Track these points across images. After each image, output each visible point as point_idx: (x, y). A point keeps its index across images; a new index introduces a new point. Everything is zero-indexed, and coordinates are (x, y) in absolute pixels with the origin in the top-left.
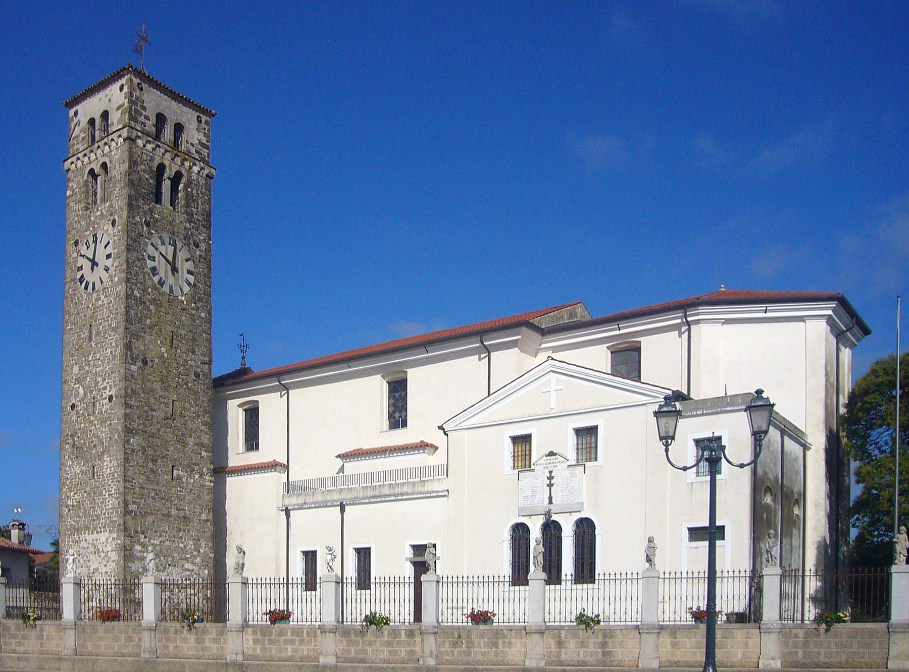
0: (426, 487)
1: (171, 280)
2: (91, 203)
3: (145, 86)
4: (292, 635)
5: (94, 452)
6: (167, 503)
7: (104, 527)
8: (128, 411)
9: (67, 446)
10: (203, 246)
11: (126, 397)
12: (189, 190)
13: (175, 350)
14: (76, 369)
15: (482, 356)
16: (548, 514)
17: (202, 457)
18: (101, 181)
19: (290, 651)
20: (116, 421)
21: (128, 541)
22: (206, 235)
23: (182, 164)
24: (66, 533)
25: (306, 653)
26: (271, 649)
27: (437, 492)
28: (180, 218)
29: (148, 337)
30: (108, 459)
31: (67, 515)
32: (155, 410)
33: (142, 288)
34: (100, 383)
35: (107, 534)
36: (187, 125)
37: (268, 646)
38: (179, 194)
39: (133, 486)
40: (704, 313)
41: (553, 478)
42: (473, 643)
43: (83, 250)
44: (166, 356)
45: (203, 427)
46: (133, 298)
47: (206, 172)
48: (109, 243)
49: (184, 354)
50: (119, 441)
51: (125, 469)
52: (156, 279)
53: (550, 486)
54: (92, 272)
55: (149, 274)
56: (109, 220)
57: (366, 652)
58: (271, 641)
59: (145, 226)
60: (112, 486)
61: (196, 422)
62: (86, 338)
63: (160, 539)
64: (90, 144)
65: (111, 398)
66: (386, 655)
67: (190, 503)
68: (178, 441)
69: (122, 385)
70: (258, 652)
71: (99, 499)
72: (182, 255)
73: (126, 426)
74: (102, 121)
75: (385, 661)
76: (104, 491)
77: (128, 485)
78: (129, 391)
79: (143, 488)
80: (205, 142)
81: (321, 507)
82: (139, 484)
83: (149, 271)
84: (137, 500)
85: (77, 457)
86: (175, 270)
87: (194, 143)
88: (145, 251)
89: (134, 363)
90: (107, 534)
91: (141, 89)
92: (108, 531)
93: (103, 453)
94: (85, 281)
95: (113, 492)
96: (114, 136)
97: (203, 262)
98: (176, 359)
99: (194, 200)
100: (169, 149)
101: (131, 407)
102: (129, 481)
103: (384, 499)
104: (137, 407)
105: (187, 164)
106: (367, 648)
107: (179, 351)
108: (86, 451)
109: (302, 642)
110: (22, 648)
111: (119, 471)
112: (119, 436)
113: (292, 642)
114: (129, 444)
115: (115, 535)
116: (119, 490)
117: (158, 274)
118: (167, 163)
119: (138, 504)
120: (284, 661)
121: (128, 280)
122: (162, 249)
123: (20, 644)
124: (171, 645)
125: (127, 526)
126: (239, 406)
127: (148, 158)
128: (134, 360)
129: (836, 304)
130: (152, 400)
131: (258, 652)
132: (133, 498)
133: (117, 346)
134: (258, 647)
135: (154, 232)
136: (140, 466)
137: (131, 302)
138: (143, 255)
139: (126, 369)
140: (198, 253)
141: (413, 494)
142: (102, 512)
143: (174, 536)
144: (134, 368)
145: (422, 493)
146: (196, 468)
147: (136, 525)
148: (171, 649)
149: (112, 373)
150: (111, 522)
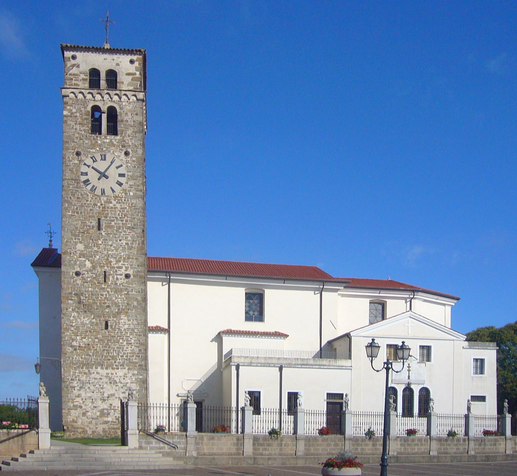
4: (418, 441)
16: (409, 384)
19: (416, 449)
25: (423, 450)
26: (408, 448)
27: (346, 367)
35: (126, 371)
37: (407, 447)
40: (420, 295)
41: (410, 367)
42: (486, 444)
53: (409, 371)
57: (447, 449)
58: (408, 445)
66: (454, 450)
70: (402, 450)
75: (455, 453)
81: (265, 366)
90: (126, 371)
106: (448, 447)
109: (422, 445)
110: (267, 452)
113: (418, 445)
115: (136, 372)
120: (414, 454)
123: (266, 450)
124: (359, 448)
129: (455, 303)
131: (402, 450)
134: (403, 448)
141: (329, 366)
148: (359, 451)
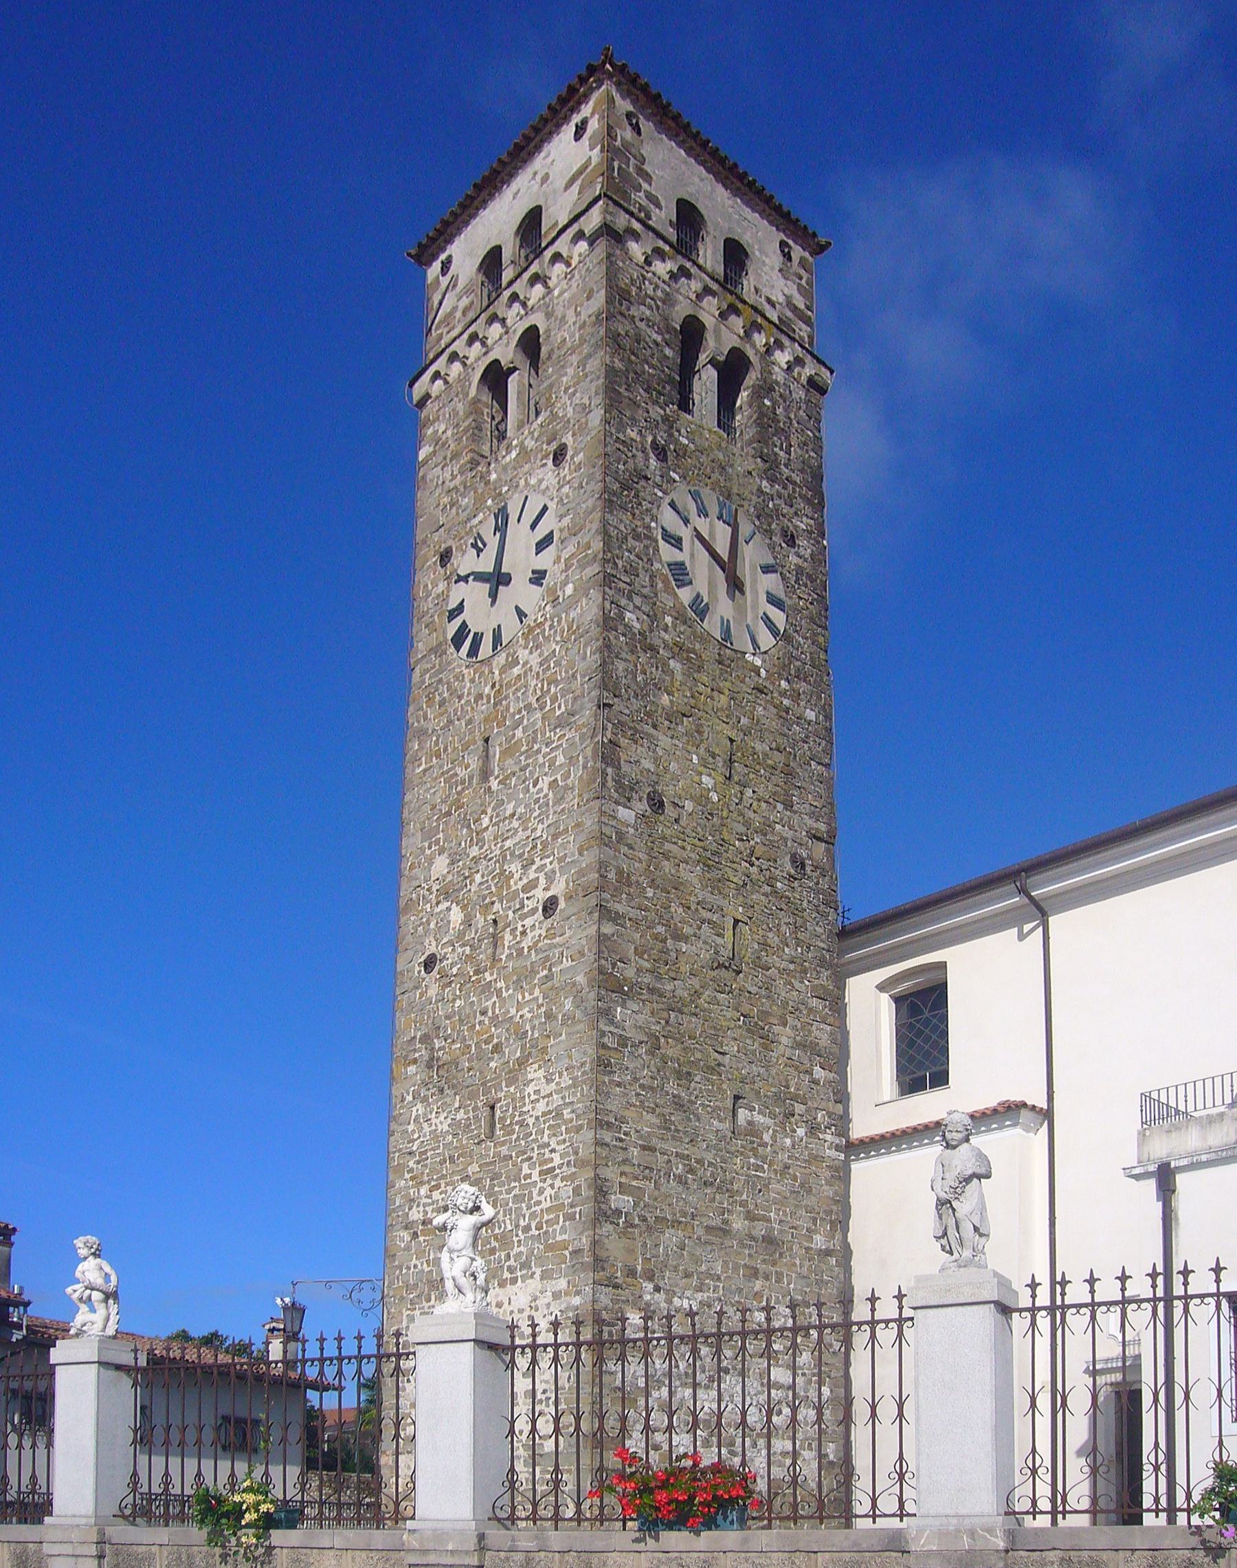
1: (724, 607)
2: (487, 454)
3: (647, 126)
5: (493, 1064)
6: (717, 1196)
7: (525, 1265)
8: (608, 929)
9: (412, 1069)
10: (805, 546)
11: (600, 889)
12: (767, 402)
13: (738, 788)
14: (441, 865)
17: (815, 1082)
18: (520, 382)
20: (566, 963)
21: (605, 1297)
22: (812, 522)
23: (748, 335)
24: (402, 1298)
28: (744, 462)
29: (664, 741)
30: (541, 1073)
31: (408, 1248)
32: (686, 939)
33: (646, 608)
34: (517, 876)
35: (534, 1284)
36: (757, 253)
38: (738, 418)
39: (621, 1140)
43: (466, 562)
44: (715, 798)
45: (814, 1002)
46: (621, 629)
47: (809, 370)
48: (545, 508)
49: (763, 805)
50: (578, 1014)
51: (600, 1091)
52: (685, 595)
54: (493, 603)
55: (666, 581)
56: (546, 456)
59: (652, 455)
60: (553, 1145)
61: (797, 985)
62: (471, 778)
63: (699, 1296)
64: (485, 303)
65: (550, 907)
67: (782, 1202)
68: (749, 1031)
69: (589, 858)
71: (509, 1192)
72: (752, 555)
73: (601, 971)
74: (521, 246)
76: (525, 1165)
77: (607, 1136)
78: (612, 875)
79: (652, 1149)
80: (802, 307)
82: (641, 1137)
83: (666, 571)
84: (634, 1183)
85: (442, 1091)
86: (735, 585)
87: (774, 298)
88: (654, 518)
89: (622, 800)
91: (637, 129)
92: (537, 1276)
93: (522, 1063)
94: (471, 635)
95: (557, 1160)
96: (562, 246)
97: (806, 586)
98: (741, 814)
99: (780, 432)
100: (715, 287)
101: (616, 918)
102: (609, 1124)
104: (636, 922)
105: (760, 339)
107: (749, 792)
108: (470, 1069)
111: (580, 1099)
112: (579, 1002)
114: (612, 1022)
115: (562, 1284)
116: (576, 1153)
117: (691, 583)
118: (708, 320)
119: (637, 1193)
121: (607, 580)
122: (702, 525)
125: (604, 1254)
126: (882, 987)
127: (659, 293)
128: (626, 792)
130: (677, 910)
132: (622, 1174)
133: (572, 761)
135: (677, 478)
136: (642, 1087)
137: (617, 638)
138: (648, 528)
139: (603, 813)
140: (793, 559)
142: (517, 1226)
143: (740, 1290)
144: (624, 814)
146: (799, 1108)
147: (631, 1251)
149: (555, 837)
150: (550, 1247)
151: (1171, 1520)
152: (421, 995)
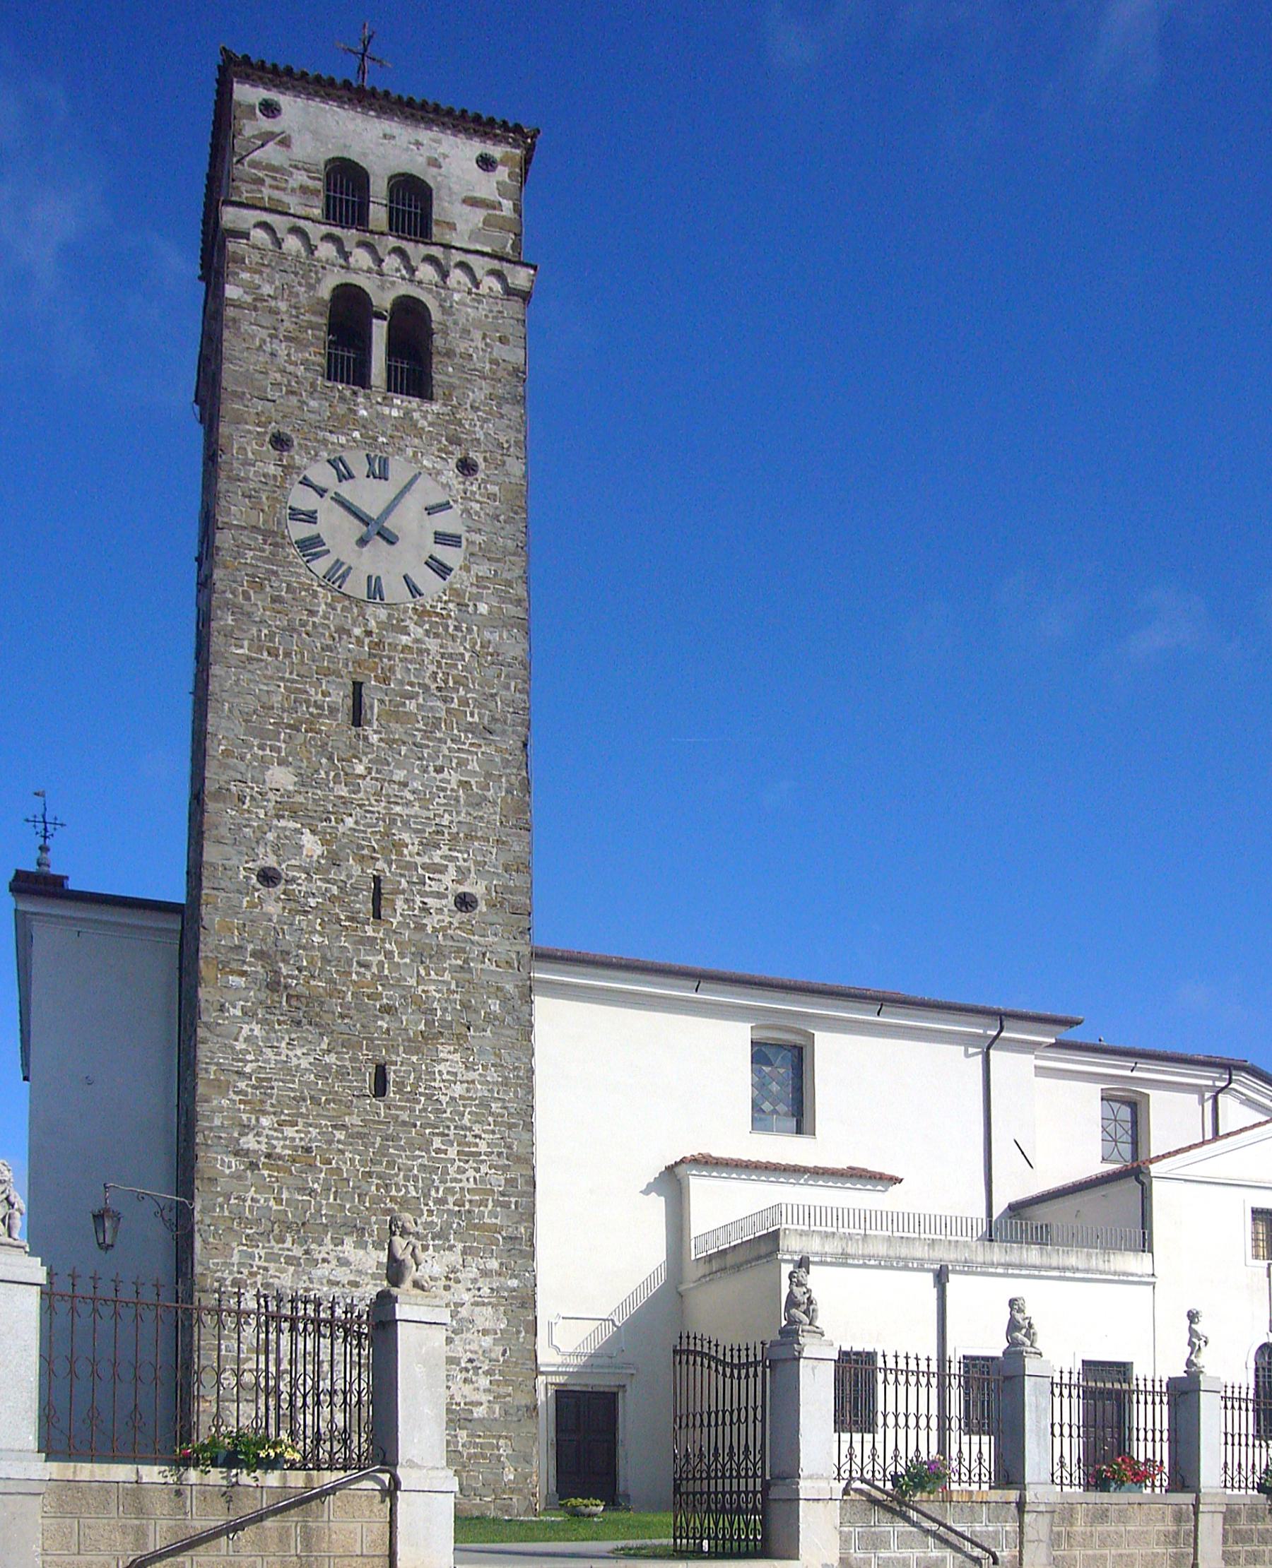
0: (1112, 1264)
15: (971, 1050)
35: (454, 1258)
95: (483, 1147)
103: (1036, 1273)
115: (494, 1264)
145: (1101, 1272)
151: (1153, 1490)
152: (252, 905)
